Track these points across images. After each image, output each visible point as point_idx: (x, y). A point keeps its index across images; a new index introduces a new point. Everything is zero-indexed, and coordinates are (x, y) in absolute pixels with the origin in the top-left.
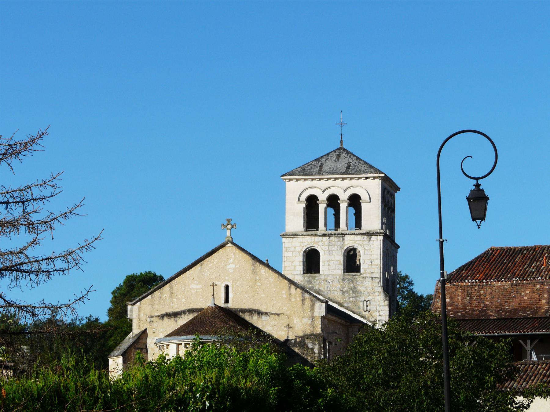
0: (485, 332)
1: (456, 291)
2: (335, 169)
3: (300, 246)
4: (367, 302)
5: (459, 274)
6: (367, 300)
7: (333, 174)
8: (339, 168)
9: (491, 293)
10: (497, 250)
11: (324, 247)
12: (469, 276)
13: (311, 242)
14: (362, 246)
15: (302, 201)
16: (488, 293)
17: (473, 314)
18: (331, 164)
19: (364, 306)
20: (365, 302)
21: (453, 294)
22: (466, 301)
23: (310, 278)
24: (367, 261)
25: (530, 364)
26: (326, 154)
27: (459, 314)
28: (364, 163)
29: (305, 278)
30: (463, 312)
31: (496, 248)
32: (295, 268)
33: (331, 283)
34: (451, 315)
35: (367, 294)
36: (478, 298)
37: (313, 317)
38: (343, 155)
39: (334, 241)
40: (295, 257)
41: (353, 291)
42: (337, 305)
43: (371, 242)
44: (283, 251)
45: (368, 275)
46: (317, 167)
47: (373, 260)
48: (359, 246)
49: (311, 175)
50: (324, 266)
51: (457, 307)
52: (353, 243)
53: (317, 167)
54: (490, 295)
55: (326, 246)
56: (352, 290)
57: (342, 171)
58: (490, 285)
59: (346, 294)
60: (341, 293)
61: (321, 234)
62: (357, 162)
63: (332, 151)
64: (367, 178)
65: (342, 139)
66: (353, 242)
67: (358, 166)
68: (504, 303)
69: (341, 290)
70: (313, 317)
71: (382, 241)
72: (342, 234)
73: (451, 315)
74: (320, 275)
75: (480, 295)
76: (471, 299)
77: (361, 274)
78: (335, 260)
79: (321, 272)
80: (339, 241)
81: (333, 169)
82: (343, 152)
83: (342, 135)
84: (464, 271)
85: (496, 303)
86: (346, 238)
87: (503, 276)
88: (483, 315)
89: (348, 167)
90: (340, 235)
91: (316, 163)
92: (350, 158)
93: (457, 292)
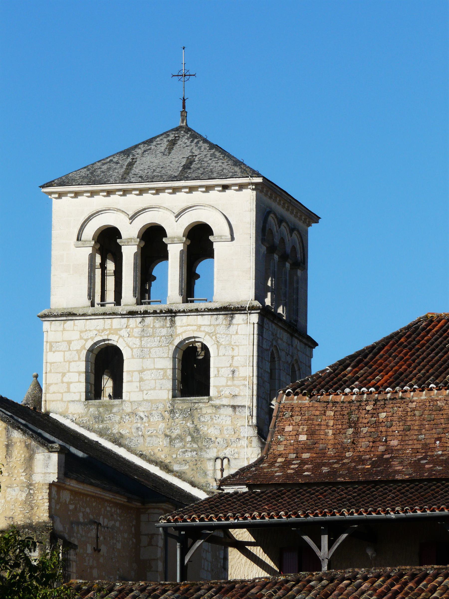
0: (366, 511)
1: (321, 414)
2: (158, 170)
3: (81, 338)
4: (222, 460)
5: (337, 375)
6: (222, 456)
7: (152, 180)
8: (168, 168)
9: (402, 419)
10: (439, 321)
11: (130, 341)
12: (357, 379)
13: (104, 330)
14: (214, 337)
15: (85, 241)
16: (395, 418)
17: (357, 470)
18: (154, 159)
19: (215, 470)
20: (219, 461)
21: (315, 423)
22: (346, 437)
23: (101, 409)
24: (223, 370)
25: (344, 579)
26: (147, 141)
27: (325, 469)
28: (224, 157)
29: (91, 410)
30: (336, 466)
31: (438, 317)
32: (68, 388)
33: (145, 419)
34: (306, 473)
35: (222, 442)
36: (373, 430)
37: (31, 485)
38: (184, 140)
39: (154, 327)
40: (70, 362)
41: (193, 437)
42: (158, 468)
43: (233, 329)
44: (45, 350)
45: (225, 402)
46: (121, 167)
47: (237, 367)
48: (207, 337)
49: (105, 183)
50: (132, 381)
51: (323, 453)
52: (193, 331)
53: (121, 167)
54: (401, 424)
55: (136, 337)
56: (190, 434)
57: (172, 173)
58: (402, 398)
59: (178, 444)
60: (166, 442)
61: (125, 312)
62: (209, 155)
63: (162, 135)
64: (225, 187)
65: (184, 107)
66: (195, 328)
67: (210, 162)
68: (433, 440)
69: (166, 436)
70: (30, 486)
71: (256, 326)
72: (170, 311)
73: (306, 473)
74: (122, 402)
75: (377, 424)
76: (356, 433)
77: (210, 399)
78: (155, 369)
79: (124, 395)
80: (163, 327)
81: (154, 170)
82: (183, 136)
83: (184, 100)
84: (349, 368)
85: (415, 442)
86: (179, 320)
87: (437, 378)
88: (379, 471)
89: (187, 167)
90: (166, 312)
91: (122, 157)
92: (196, 146)
93: (324, 417)
